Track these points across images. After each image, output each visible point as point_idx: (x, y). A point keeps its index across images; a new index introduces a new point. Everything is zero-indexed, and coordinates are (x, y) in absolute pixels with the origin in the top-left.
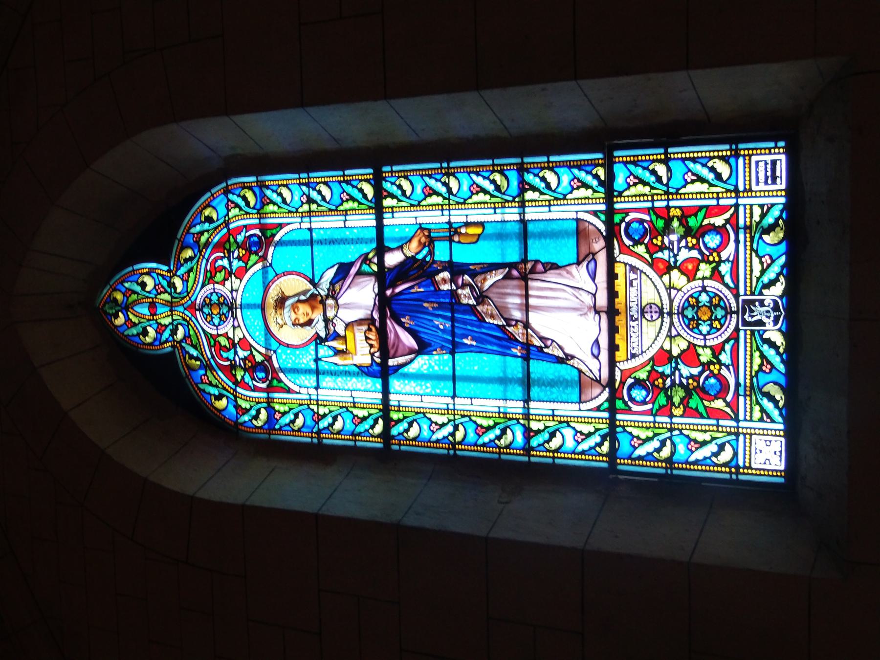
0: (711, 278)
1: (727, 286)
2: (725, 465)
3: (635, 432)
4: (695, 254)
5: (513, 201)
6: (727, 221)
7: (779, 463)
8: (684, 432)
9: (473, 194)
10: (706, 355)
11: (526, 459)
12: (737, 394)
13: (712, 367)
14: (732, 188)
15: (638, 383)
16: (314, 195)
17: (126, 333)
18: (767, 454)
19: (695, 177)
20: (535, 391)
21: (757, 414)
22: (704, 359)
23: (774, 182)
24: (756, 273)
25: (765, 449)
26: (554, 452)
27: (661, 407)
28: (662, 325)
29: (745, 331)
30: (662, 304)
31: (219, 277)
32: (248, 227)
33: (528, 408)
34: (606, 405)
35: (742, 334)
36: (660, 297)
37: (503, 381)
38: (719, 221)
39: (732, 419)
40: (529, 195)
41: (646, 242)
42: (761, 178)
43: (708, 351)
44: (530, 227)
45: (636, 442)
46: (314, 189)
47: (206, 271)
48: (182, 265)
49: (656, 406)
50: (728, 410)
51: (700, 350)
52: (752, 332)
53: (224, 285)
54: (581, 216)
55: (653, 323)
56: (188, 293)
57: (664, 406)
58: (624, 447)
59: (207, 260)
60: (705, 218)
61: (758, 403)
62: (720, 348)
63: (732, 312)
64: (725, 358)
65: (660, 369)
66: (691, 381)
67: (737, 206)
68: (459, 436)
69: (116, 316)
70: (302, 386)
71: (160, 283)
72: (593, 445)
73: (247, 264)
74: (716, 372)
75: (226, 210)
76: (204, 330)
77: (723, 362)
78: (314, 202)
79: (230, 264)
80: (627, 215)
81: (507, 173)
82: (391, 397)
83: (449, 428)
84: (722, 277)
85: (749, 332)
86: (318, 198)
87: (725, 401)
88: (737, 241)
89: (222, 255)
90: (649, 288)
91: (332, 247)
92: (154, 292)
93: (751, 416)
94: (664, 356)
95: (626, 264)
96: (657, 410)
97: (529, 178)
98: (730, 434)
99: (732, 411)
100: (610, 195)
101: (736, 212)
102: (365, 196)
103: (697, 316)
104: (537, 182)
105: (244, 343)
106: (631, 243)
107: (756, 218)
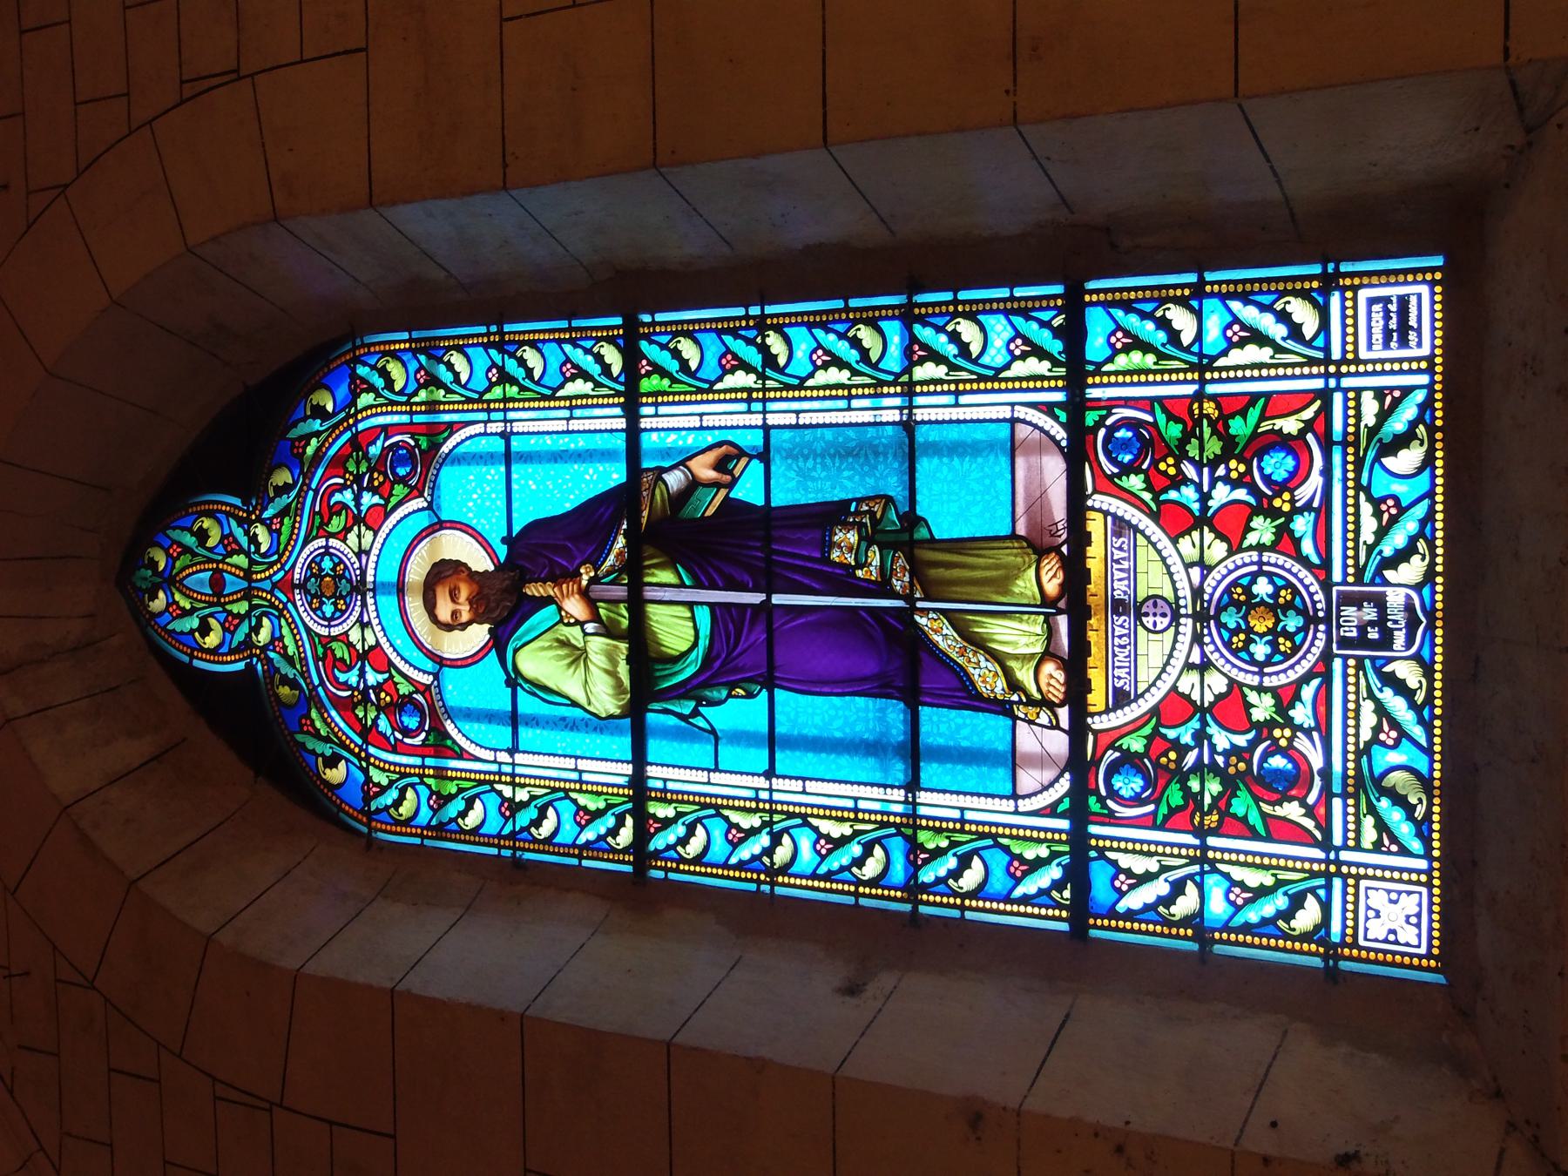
0: (1273, 548)
1: (1304, 561)
2: (1305, 937)
3: (1125, 861)
4: (1241, 494)
5: (894, 384)
6: (1309, 426)
7: (1415, 942)
8: (1219, 866)
9: (816, 368)
10: (1263, 708)
11: (908, 907)
12: (1327, 794)
13: (1277, 733)
14: (1320, 355)
15: (1129, 761)
16: (511, 366)
17: (170, 627)
18: (1395, 917)
19: (1236, 335)
20: (931, 773)
21: (1369, 835)
22: (1258, 715)
23: (1403, 343)
24: (1367, 535)
25: (1386, 909)
26: (964, 896)
27: (1173, 811)
28: (1175, 641)
29: (1345, 658)
30: (1177, 598)
31: (336, 524)
32: (387, 430)
33: (915, 804)
34: (1066, 805)
35: (1337, 664)
36: (1173, 583)
37: (871, 748)
38: (1290, 425)
39: (1314, 843)
40: (927, 371)
41: (1145, 466)
42: (1383, 333)
43: (1268, 700)
44: (922, 434)
45: (1122, 882)
46: (512, 355)
47: (313, 513)
48: (272, 500)
49: (1163, 810)
50: (1309, 824)
51: (1252, 697)
52: (1360, 662)
53: (344, 540)
54: (1021, 412)
55: (1159, 637)
56: (281, 556)
57: (1179, 809)
58: (1101, 891)
59: (316, 492)
60: (1263, 418)
61: (1372, 810)
62: (1296, 688)
63: (1315, 621)
64: (1302, 714)
65: (1171, 734)
66: (1233, 760)
67: (1325, 395)
68: (782, 854)
69: (154, 597)
70: (480, 744)
71: (231, 534)
72: (1151, 899)
73: (387, 501)
74: (1283, 743)
75: (382, 393)
76: (308, 630)
77: (1297, 721)
78: (513, 381)
79: (357, 499)
80: (1110, 414)
81: (883, 324)
82: (651, 771)
83: (764, 840)
84: (1297, 542)
85: (1351, 662)
86: (519, 373)
87: (1303, 804)
88: (1327, 472)
89: (341, 481)
90: (1158, 565)
91: (559, 467)
92: (221, 549)
93: (1358, 839)
94: (1177, 706)
95: (1106, 513)
96: (1166, 818)
97: (924, 333)
98: (1313, 875)
99: (1318, 826)
100: (1077, 370)
101: (1326, 409)
102: (606, 369)
103: (1247, 623)
104: (941, 343)
105: (372, 656)
106: (1116, 470)
107: (1369, 419)
